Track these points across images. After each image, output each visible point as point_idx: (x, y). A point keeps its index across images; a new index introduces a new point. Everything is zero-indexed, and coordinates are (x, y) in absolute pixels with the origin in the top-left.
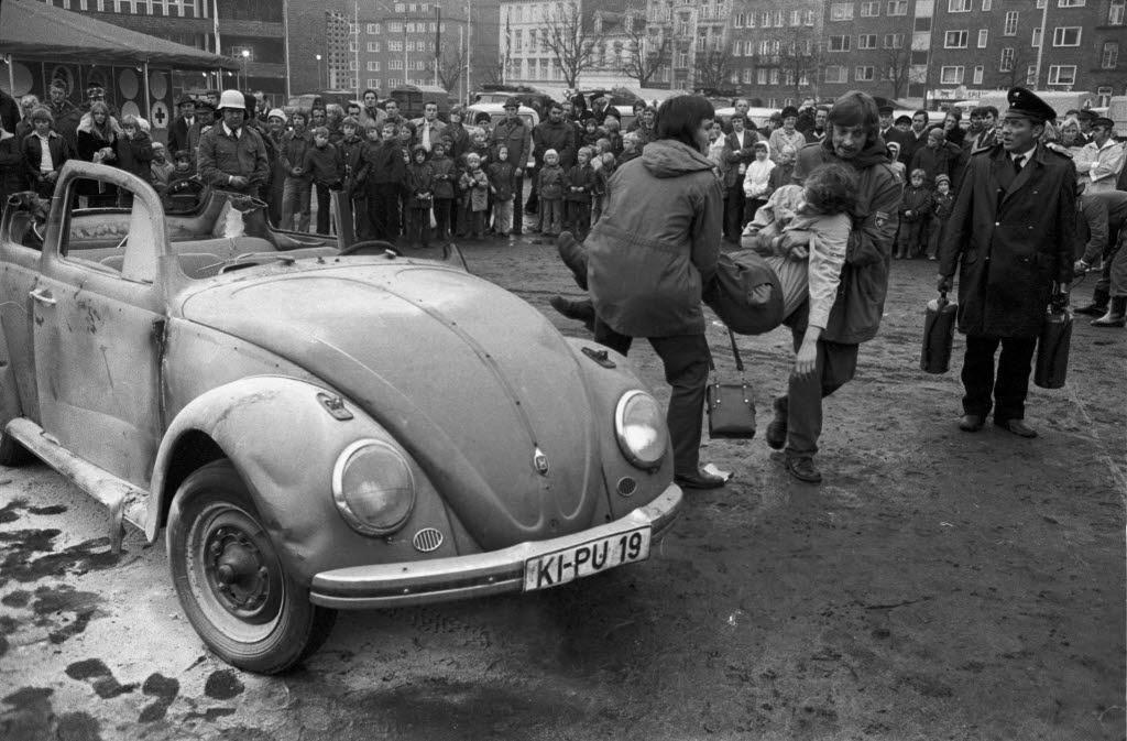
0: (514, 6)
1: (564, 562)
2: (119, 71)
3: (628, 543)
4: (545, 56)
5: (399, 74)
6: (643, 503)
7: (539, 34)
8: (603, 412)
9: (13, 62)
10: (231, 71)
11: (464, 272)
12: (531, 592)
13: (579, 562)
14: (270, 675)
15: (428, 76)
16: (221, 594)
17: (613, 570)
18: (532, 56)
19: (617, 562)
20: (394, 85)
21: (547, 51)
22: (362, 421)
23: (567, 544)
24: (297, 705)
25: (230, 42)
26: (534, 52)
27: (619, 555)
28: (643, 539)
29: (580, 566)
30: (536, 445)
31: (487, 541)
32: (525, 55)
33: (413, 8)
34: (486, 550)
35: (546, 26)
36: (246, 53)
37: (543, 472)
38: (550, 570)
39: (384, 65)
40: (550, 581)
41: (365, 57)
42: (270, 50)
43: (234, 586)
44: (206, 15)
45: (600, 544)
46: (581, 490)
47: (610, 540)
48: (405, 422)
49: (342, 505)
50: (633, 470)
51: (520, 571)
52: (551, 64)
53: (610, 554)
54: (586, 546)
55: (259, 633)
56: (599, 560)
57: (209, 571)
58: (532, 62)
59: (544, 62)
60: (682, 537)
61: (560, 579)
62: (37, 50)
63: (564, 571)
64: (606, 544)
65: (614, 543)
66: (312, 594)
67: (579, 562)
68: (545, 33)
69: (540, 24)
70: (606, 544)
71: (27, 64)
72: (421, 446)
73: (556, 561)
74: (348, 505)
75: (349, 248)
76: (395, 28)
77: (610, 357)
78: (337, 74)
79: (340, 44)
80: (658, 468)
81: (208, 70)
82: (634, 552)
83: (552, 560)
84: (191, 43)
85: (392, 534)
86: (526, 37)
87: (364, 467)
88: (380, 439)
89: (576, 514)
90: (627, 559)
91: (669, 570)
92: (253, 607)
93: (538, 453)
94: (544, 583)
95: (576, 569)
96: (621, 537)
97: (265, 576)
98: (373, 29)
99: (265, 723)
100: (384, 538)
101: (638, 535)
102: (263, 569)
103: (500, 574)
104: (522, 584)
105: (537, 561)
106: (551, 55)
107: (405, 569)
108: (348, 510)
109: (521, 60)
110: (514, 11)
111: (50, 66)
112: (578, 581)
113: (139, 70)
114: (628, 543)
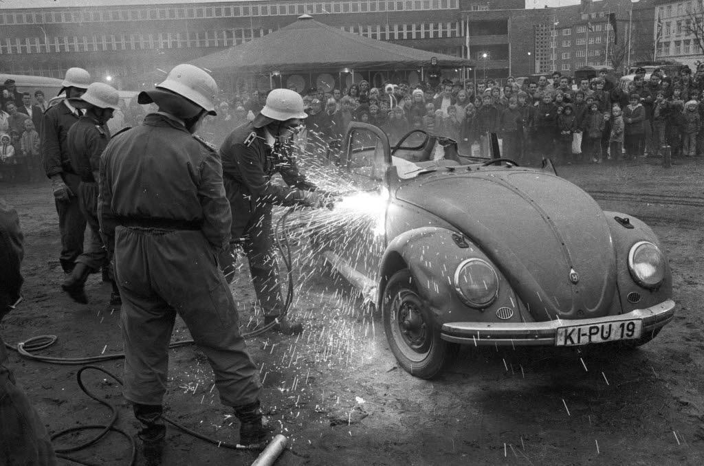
0: (665, 7)
1: (582, 333)
2: (408, 72)
3: (625, 327)
4: (688, 38)
5: (582, 60)
6: (642, 307)
7: (683, 23)
8: (621, 251)
9: (355, 72)
10: (471, 67)
11: (554, 175)
12: (561, 347)
13: (591, 334)
14: (426, 379)
15: (601, 60)
16: (405, 336)
17: (615, 342)
18: (678, 39)
19: (618, 338)
20: (578, 66)
21: (689, 34)
22: (472, 249)
23: (585, 324)
24: (436, 393)
25: (475, 49)
26: (679, 36)
27: (619, 334)
28: (636, 326)
29: (592, 336)
30: (571, 268)
31: (538, 316)
32: (673, 38)
33: (593, 16)
34: (537, 321)
35: (688, 17)
36: (485, 55)
37: (575, 283)
38: (572, 336)
39: (573, 55)
40: (573, 342)
41: (559, 51)
42: (500, 52)
43: (411, 331)
44: (463, 35)
45: (607, 326)
46: (600, 295)
47: (613, 324)
48: (497, 251)
49: (458, 290)
50: (638, 288)
51: (554, 334)
52: (692, 42)
53: (613, 333)
54: (597, 325)
55: (422, 357)
56: (605, 335)
57: (400, 324)
58: (678, 43)
59: (687, 42)
60: (688, 340)
61: (579, 342)
62: (366, 65)
63: (582, 338)
64: (610, 326)
65: (615, 326)
66: (443, 334)
67: (591, 334)
68: (688, 22)
69: (684, 16)
70: (610, 326)
71: (361, 73)
72: (503, 263)
73: (577, 331)
74: (461, 290)
75: (495, 160)
76: (581, 30)
77: (631, 222)
78: (541, 63)
79: (543, 45)
80: (658, 289)
81: (458, 68)
82: (630, 333)
83: (573, 330)
84: (453, 52)
85: (486, 307)
86: (674, 27)
87: (473, 270)
88: (482, 259)
89: (596, 308)
90: (625, 337)
91: (672, 357)
92: (418, 345)
93: (572, 271)
94: (569, 343)
95: (590, 338)
96: (621, 323)
97: (424, 327)
98: (567, 32)
99: (419, 400)
100: (479, 309)
101: (633, 324)
102: (424, 324)
103: (542, 334)
104: (555, 341)
105: (564, 329)
106: (693, 36)
107: (489, 326)
108: (461, 293)
109: (669, 42)
110: (665, 11)
111: (372, 74)
112: (591, 346)
113: (419, 71)
114: (625, 327)
